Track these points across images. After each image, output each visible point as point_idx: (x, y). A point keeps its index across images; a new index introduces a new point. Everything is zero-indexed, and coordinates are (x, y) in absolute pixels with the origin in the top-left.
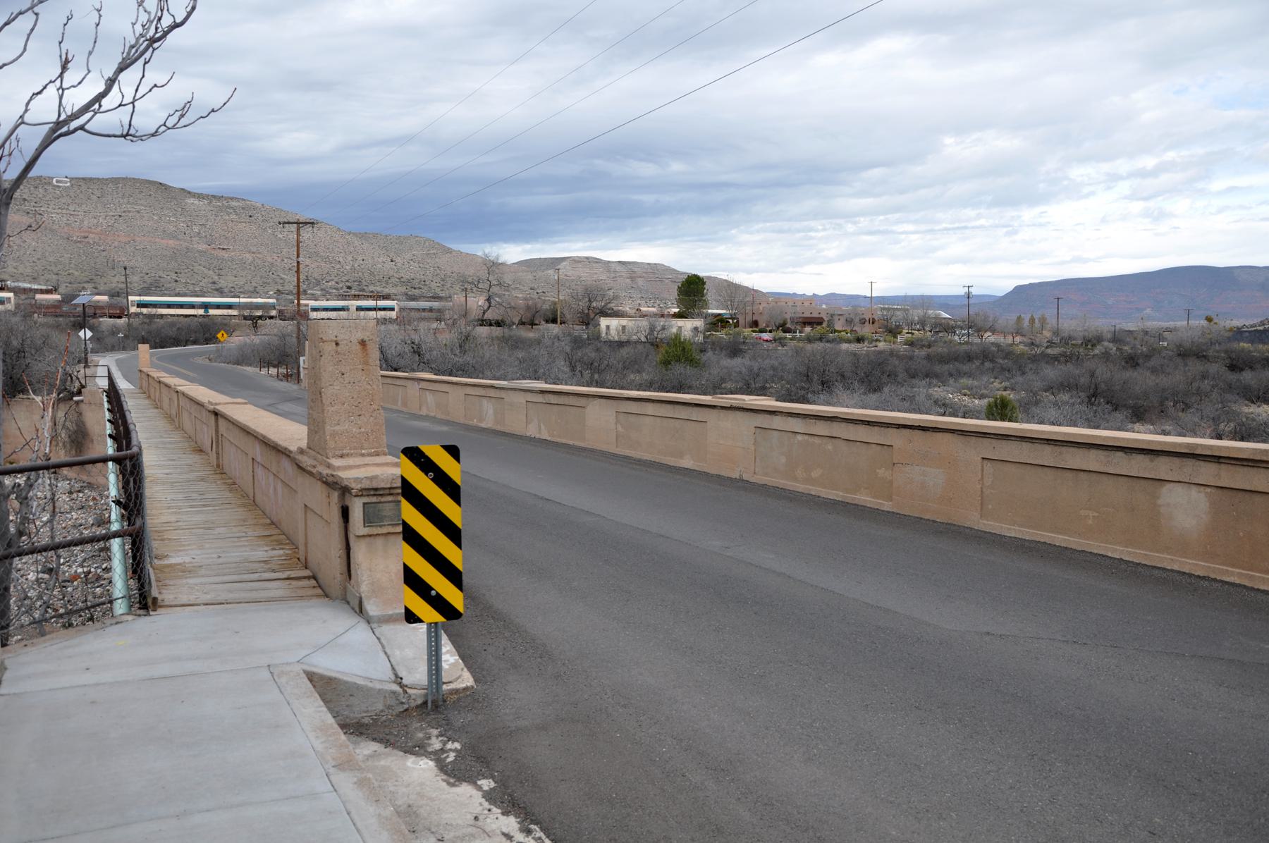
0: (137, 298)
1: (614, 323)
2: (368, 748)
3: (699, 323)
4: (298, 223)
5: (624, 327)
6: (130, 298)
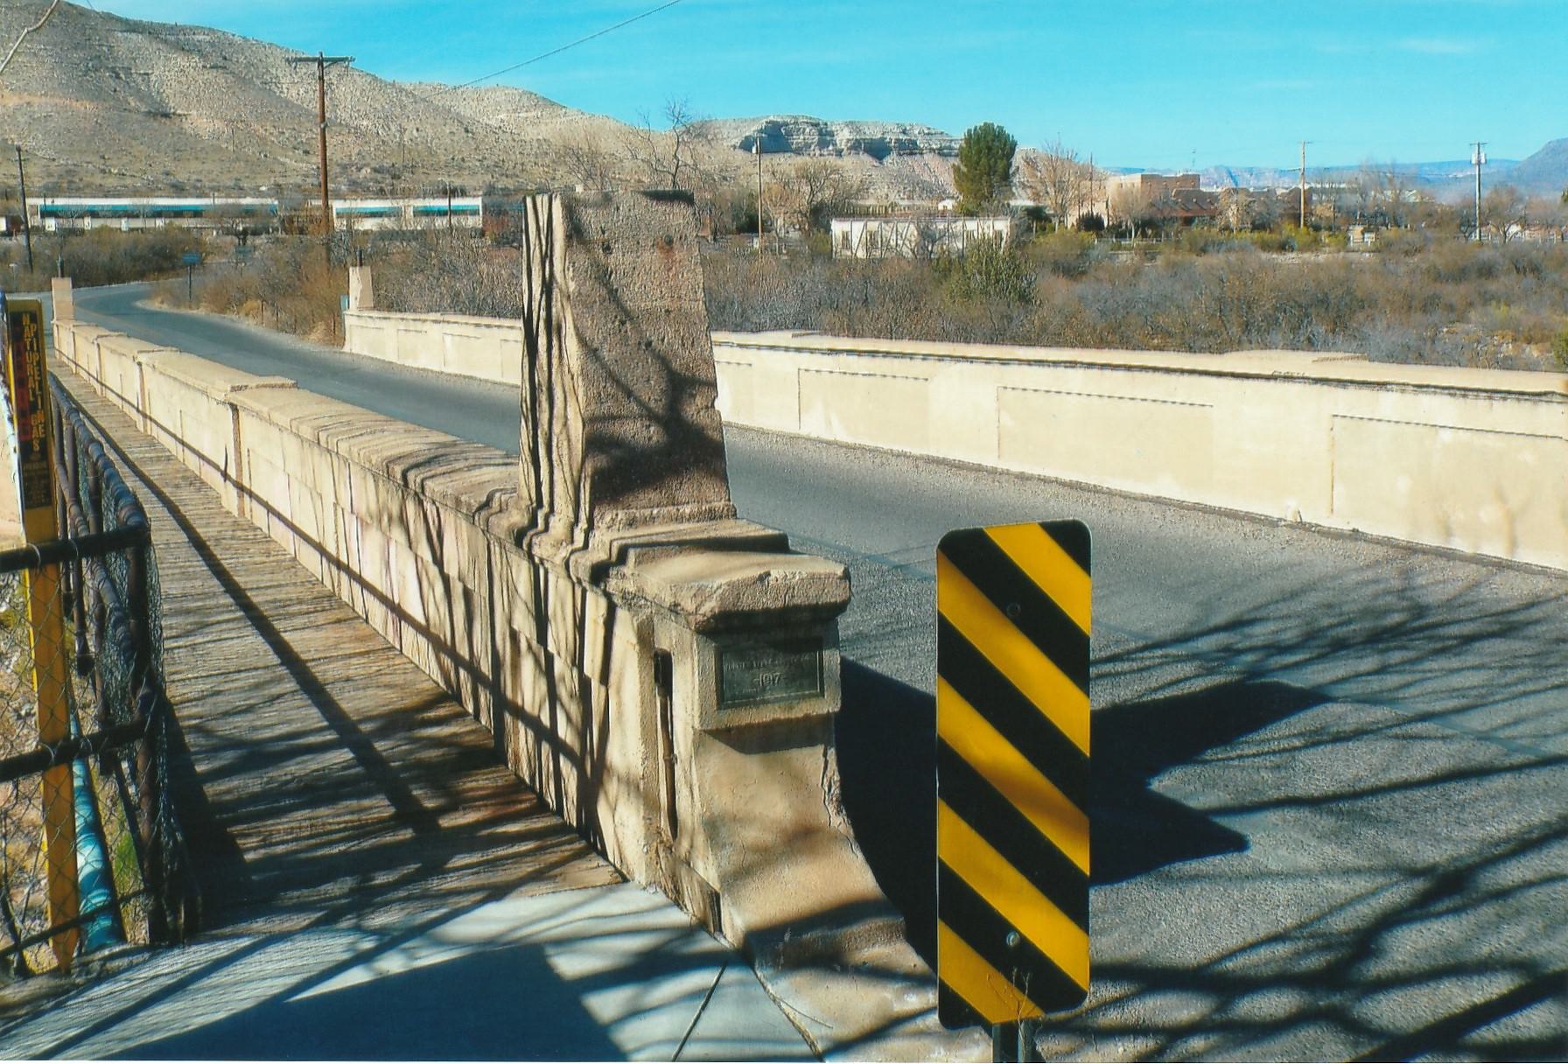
0: (40, 202)
1: (856, 229)
2: (1429, 539)
3: (1003, 225)
4: (321, 62)
5: (872, 235)
6: (29, 201)
